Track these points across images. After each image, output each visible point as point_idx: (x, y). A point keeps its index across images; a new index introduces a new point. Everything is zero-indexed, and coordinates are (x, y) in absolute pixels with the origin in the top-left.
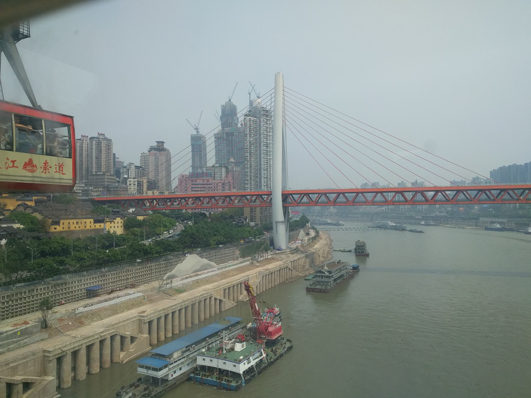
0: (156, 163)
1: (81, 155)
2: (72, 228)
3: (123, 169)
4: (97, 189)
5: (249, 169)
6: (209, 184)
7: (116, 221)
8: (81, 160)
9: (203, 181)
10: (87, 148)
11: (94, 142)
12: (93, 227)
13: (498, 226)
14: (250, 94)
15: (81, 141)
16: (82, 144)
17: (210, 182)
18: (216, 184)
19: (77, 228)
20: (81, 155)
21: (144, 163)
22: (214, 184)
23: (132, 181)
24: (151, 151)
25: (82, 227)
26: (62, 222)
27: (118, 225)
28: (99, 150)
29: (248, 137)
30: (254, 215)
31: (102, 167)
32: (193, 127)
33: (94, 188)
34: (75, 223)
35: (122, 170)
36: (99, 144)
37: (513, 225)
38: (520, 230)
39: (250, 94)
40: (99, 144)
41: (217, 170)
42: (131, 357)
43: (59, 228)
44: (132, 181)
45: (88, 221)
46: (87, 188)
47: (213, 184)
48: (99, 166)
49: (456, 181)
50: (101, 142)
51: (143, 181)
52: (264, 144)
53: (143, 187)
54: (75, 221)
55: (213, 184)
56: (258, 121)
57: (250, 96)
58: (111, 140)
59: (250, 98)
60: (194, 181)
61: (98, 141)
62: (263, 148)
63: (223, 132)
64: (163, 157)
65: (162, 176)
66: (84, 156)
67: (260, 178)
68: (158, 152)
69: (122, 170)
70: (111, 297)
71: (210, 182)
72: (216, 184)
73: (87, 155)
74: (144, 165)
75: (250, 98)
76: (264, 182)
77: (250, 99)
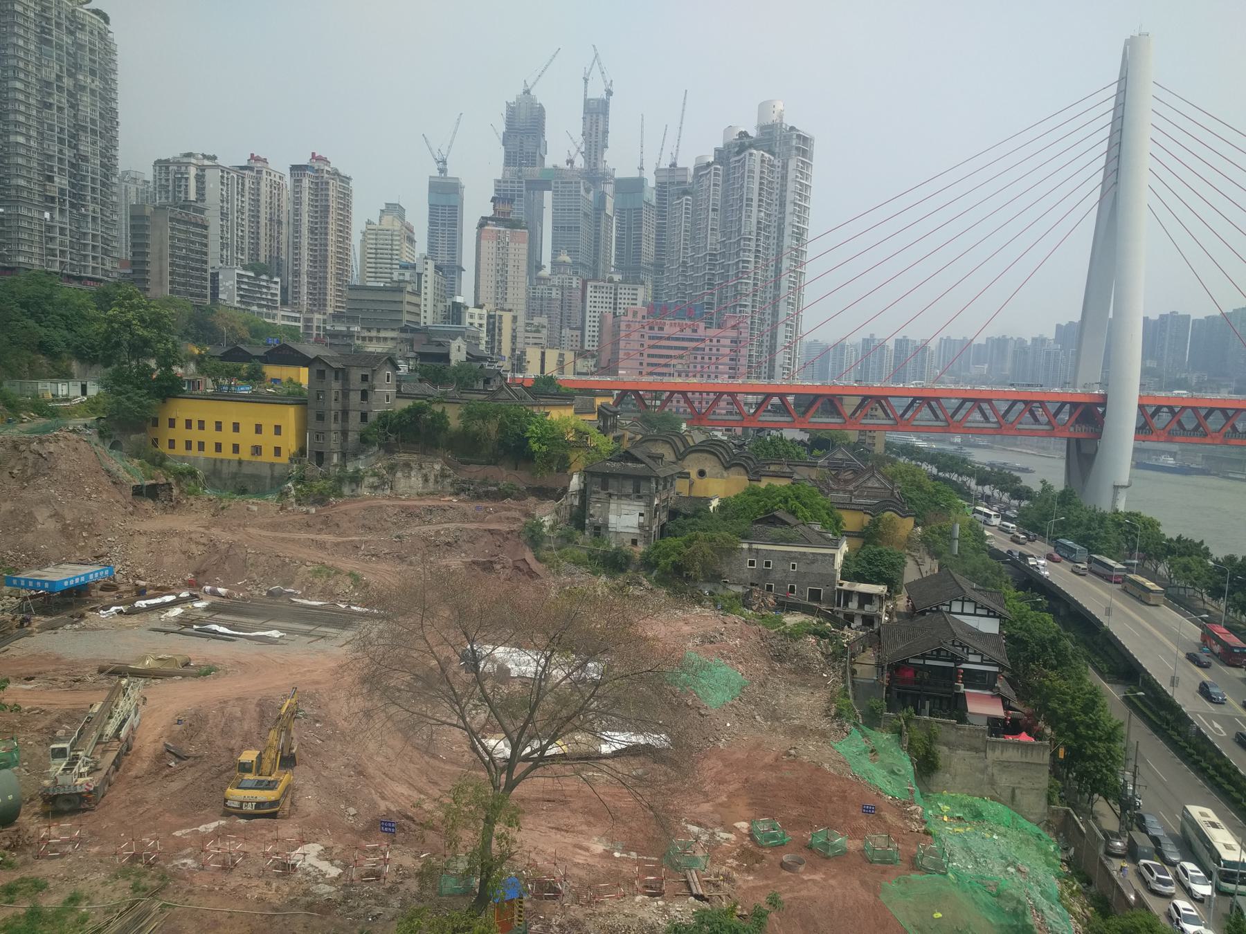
0: (501, 262)
1: (253, 216)
3: (402, 271)
4: (374, 334)
5: (750, 299)
6: (697, 340)
8: (253, 233)
10: (271, 198)
11: (306, 183)
13: (1171, 461)
14: (586, 80)
15: (254, 174)
16: (258, 183)
17: (701, 332)
18: (715, 340)
20: (253, 216)
21: (373, 251)
23: (476, 316)
24: (487, 225)
28: (321, 211)
29: (755, 209)
30: (868, 441)
31: (329, 260)
32: (433, 156)
33: (362, 328)
35: (400, 274)
36: (320, 188)
37: (1199, 460)
38: (1231, 475)
39: (586, 80)
40: (320, 188)
41: (623, 291)
44: (476, 316)
46: (344, 329)
48: (319, 258)
49: (953, 338)
50: (327, 183)
51: (501, 317)
52: (793, 232)
53: (500, 335)
56: (780, 164)
57: (586, 87)
58: (349, 179)
59: (586, 91)
60: (656, 328)
61: (317, 178)
62: (788, 241)
63: (520, 178)
64: (522, 245)
65: (515, 301)
66: (263, 221)
67: (774, 326)
68: (508, 231)
69: (400, 274)
71: (701, 332)
72: (715, 340)
73: (271, 220)
74: (373, 256)
75: (586, 91)
76: (786, 337)
77: (585, 95)
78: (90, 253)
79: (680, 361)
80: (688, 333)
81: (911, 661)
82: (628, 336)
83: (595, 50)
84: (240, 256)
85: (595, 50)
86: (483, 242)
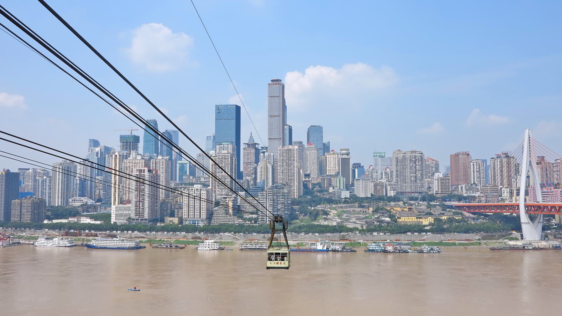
2: (406, 220)
7: (428, 218)
9: (548, 190)
12: (416, 220)
17: (552, 190)
19: (408, 221)
22: (555, 192)
25: (411, 220)
26: (401, 218)
27: (213, 245)
34: (407, 219)
42: (159, 147)
43: (400, 220)
45: (413, 218)
47: (554, 192)
54: (407, 218)
55: (554, 192)
70: (48, 185)
72: (556, 192)
78: (418, 188)
79: (548, 198)
80: (549, 191)
81: (508, 240)
82: (530, 192)
83: (251, 135)
84: (483, 180)
85: (251, 135)
86: (91, 163)
